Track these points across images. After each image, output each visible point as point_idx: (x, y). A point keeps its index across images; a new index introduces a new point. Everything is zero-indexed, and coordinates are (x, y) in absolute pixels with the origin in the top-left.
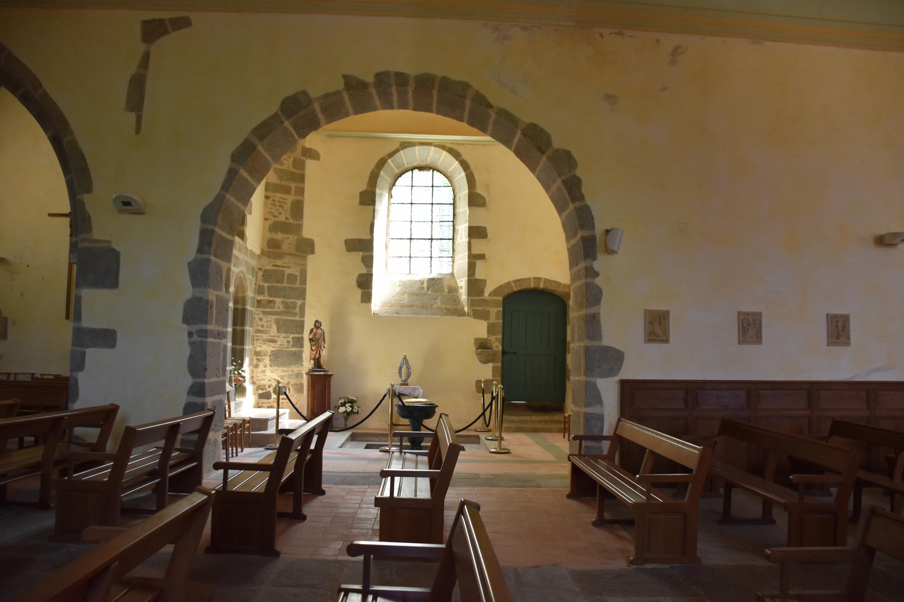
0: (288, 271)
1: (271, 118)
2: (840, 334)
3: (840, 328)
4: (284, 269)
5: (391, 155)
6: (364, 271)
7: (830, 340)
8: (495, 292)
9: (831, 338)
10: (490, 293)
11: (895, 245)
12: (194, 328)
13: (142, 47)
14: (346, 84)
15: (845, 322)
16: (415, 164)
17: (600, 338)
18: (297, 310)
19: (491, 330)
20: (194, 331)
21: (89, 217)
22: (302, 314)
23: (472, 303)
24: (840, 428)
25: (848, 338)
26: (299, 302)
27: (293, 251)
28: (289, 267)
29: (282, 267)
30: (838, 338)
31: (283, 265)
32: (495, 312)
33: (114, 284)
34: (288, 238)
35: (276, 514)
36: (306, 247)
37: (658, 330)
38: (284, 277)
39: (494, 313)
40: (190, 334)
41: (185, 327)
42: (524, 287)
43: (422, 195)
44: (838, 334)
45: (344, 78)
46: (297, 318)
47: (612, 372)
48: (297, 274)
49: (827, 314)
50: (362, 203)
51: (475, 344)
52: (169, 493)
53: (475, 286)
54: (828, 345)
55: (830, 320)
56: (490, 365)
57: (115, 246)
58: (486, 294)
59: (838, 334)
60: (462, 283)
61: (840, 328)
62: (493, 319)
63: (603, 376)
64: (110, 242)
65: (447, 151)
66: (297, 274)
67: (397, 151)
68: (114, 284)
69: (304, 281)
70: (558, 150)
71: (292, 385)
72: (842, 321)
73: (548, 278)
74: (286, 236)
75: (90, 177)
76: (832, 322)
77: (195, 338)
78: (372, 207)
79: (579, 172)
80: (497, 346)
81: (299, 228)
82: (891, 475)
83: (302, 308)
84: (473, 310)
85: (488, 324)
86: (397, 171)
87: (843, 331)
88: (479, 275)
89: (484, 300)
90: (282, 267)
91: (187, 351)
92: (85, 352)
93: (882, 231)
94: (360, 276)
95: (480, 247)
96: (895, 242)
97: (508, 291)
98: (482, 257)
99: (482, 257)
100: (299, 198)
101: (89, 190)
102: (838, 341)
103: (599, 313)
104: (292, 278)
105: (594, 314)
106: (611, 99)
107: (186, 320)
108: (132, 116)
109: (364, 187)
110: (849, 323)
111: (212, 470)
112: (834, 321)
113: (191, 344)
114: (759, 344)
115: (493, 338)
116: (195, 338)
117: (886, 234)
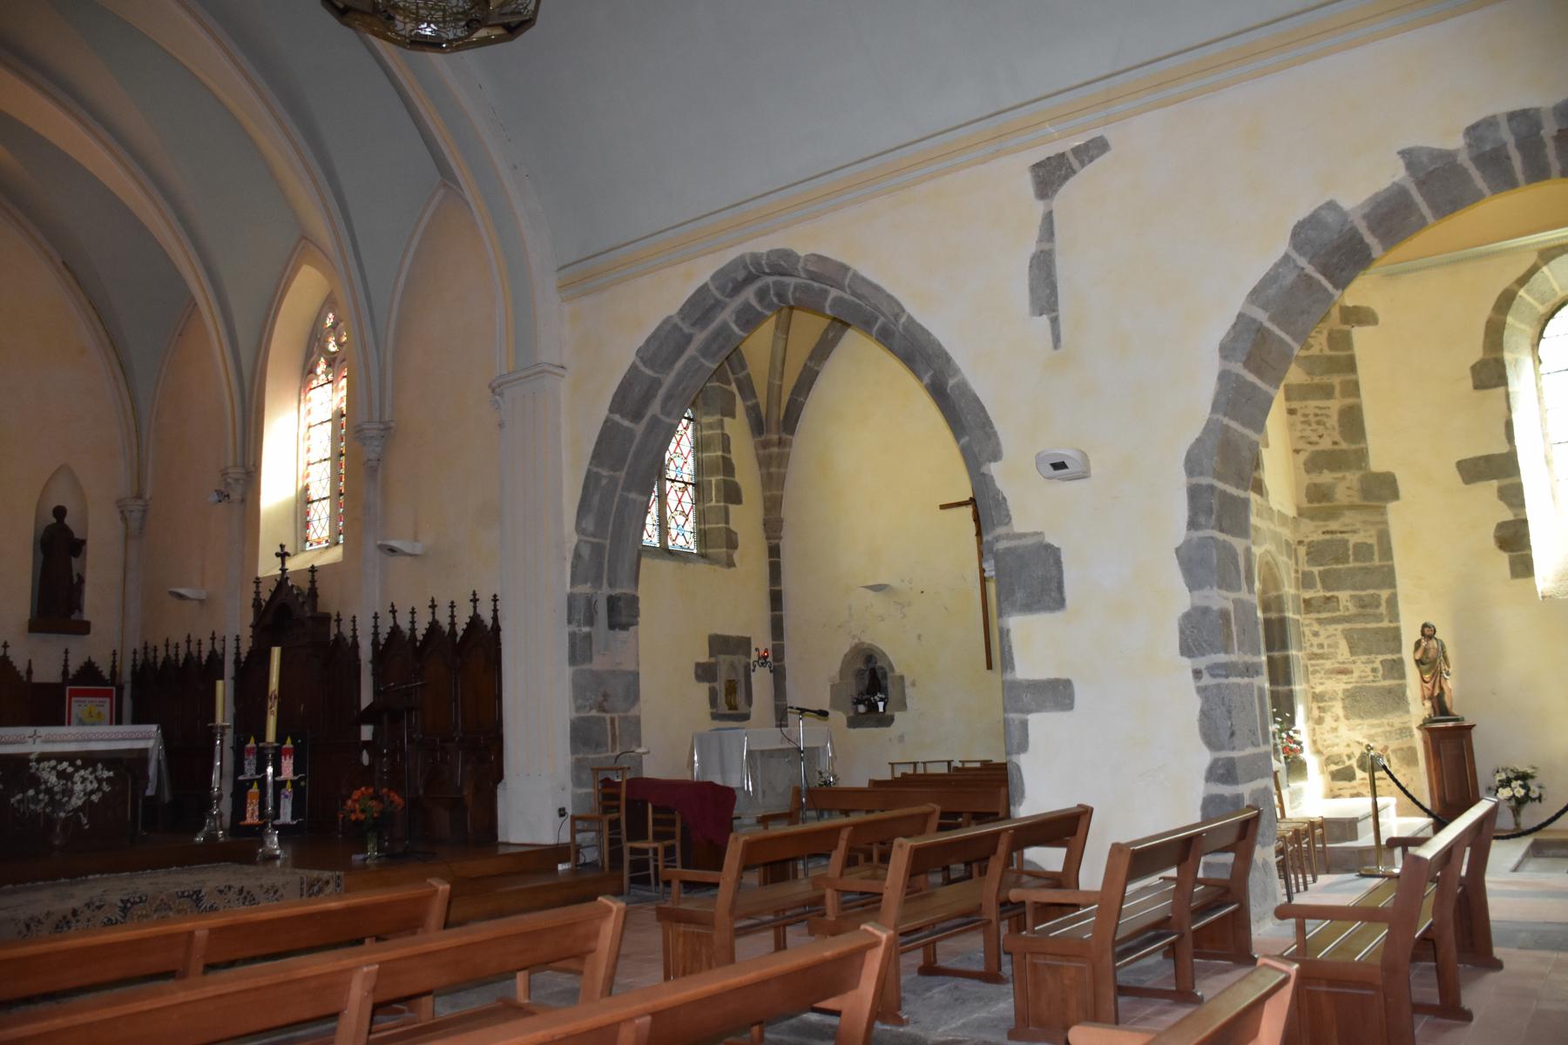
0: (1353, 539)
1: (1277, 266)
4: (1345, 536)
5: (1523, 281)
6: (1508, 515)
12: (1203, 662)
13: (1040, 207)
14: (1410, 166)
18: (1383, 609)
20: (1202, 667)
21: (1004, 499)
22: (1394, 615)
26: (1384, 594)
27: (1357, 500)
28: (1354, 532)
29: (1342, 532)
31: (1342, 529)
33: (1059, 603)
34: (1344, 478)
36: (1382, 489)
38: (1348, 550)
40: (1197, 674)
41: (1187, 664)
45: (1403, 157)
46: (1385, 624)
48: (1373, 541)
50: (1480, 385)
57: (1050, 539)
64: (1041, 533)
65: (1546, 263)
66: (1373, 541)
68: (1059, 603)
69: (1387, 552)
71: (1394, 751)
74: (1339, 475)
75: (995, 434)
77: (1207, 680)
78: (1501, 390)
81: (1361, 457)
83: (1392, 602)
86: (1543, 309)
90: (1342, 532)
91: (1196, 703)
92: (1027, 720)
94: (1501, 526)
100: (1046, 246)
101: (996, 456)
104: (1363, 551)
107: (1187, 650)
108: (1044, 320)
113: (1201, 691)
116: (1207, 680)
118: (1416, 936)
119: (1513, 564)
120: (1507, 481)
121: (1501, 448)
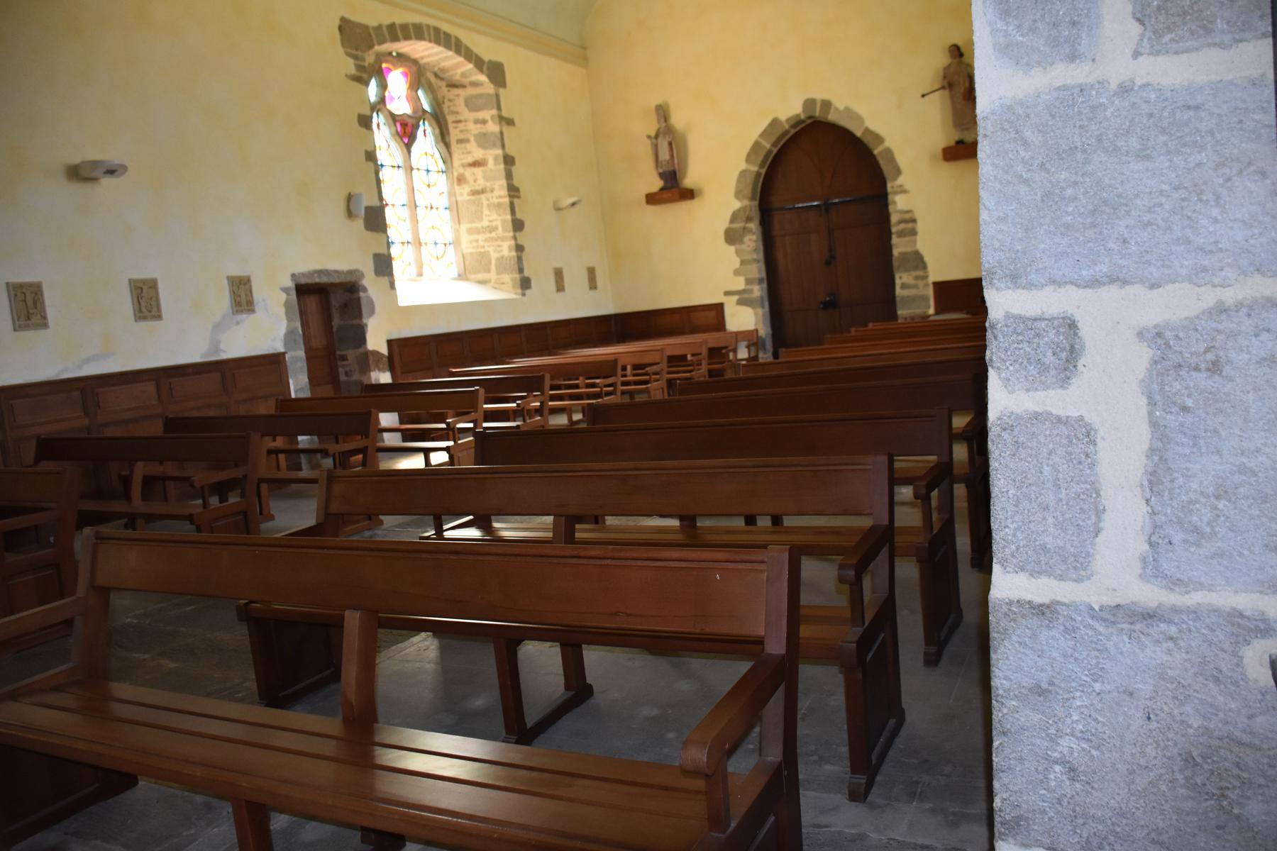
2: (31, 311)
3: (30, 303)
7: (17, 323)
9: (18, 320)
11: (94, 180)
15: (36, 294)
24: (50, 448)
25: (44, 317)
30: (29, 319)
35: (221, 505)
44: (28, 312)
49: (7, 284)
52: (551, 392)
54: (15, 330)
55: (12, 293)
59: (28, 312)
61: (30, 303)
72: (32, 293)
76: (16, 295)
82: (128, 498)
87: (35, 307)
93: (76, 159)
96: (94, 175)
102: (29, 322)
109: (514, 169)
110: (42, 295)
111: (756, 325)
112: (18, 294)
114: (45, 329)
117: (83, 162)
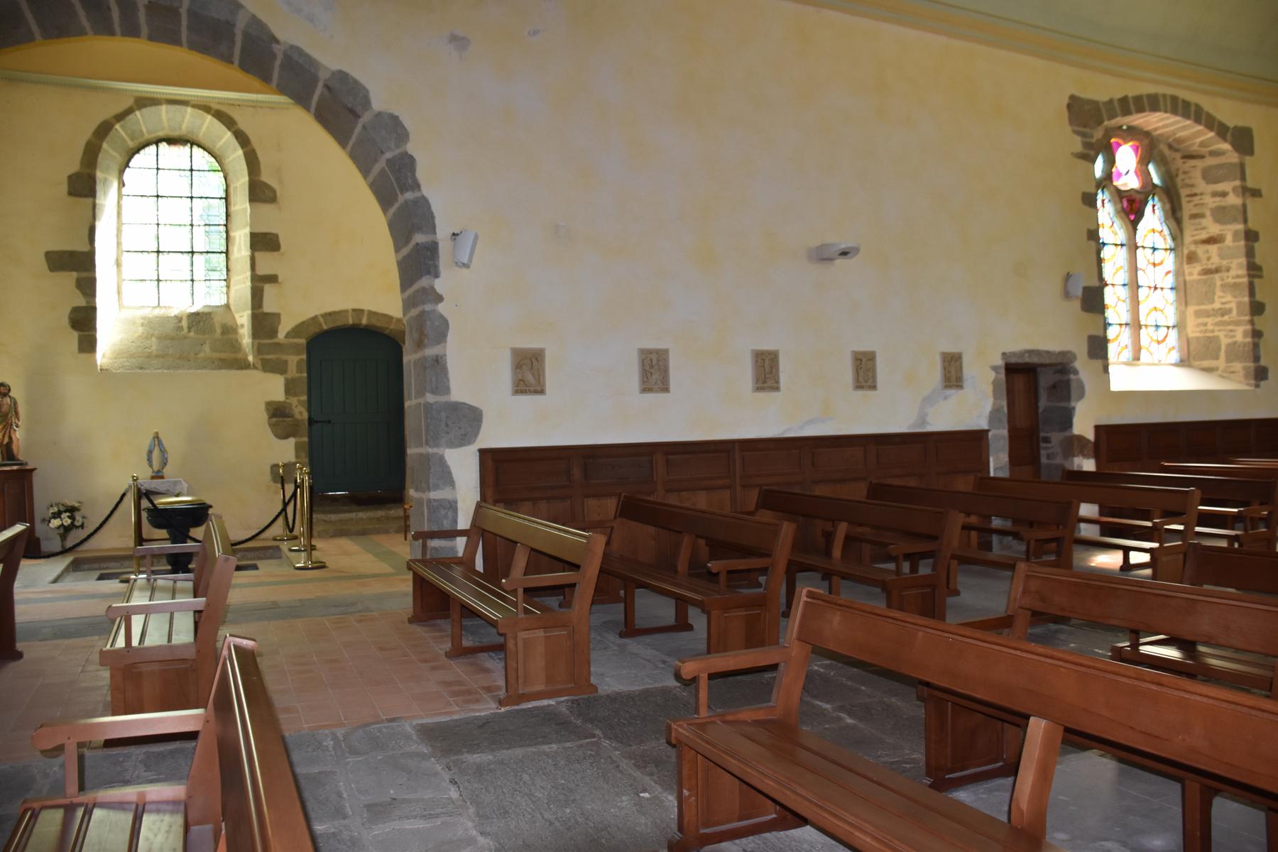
5: (121, 117)
6: (81, 302)
8: (295, 332)
10: (288, 334)
16: (161, 134)
17: (447, 390)
19: (290, 388)
23: (259, 350)
32: (295, 362)
37: (530, 378)
39: (295, 362)
42: (339, 323)
43: (175, 183)
47: (466, 438)
51: (267, 410)
53: (263, 323)
56: (292, 441)
58: (281, 335)
60: (243, 319)
62: (293, 371)
63: (452, 445)
67: (129, 111)
70: (379, 114)
73: (373, 309)
78: (89, 200)
79: (411, 148)
80: (301, 413)
84: (262, 360)
85: (286, 380)
86: (131, 144)
88: (268, 307)
89: (278, 344)
94: (76, 310)
95: (268, 263)
97: (314, 330)
98: (272, 279)
99: (272, 279)
103: (445, 355)
105: (437, 356)
106: (459, 42)
115: (294, 401)
118: (1236, 510)
119: (81, 341)
120: (84, 275)
121: (83, 247)
